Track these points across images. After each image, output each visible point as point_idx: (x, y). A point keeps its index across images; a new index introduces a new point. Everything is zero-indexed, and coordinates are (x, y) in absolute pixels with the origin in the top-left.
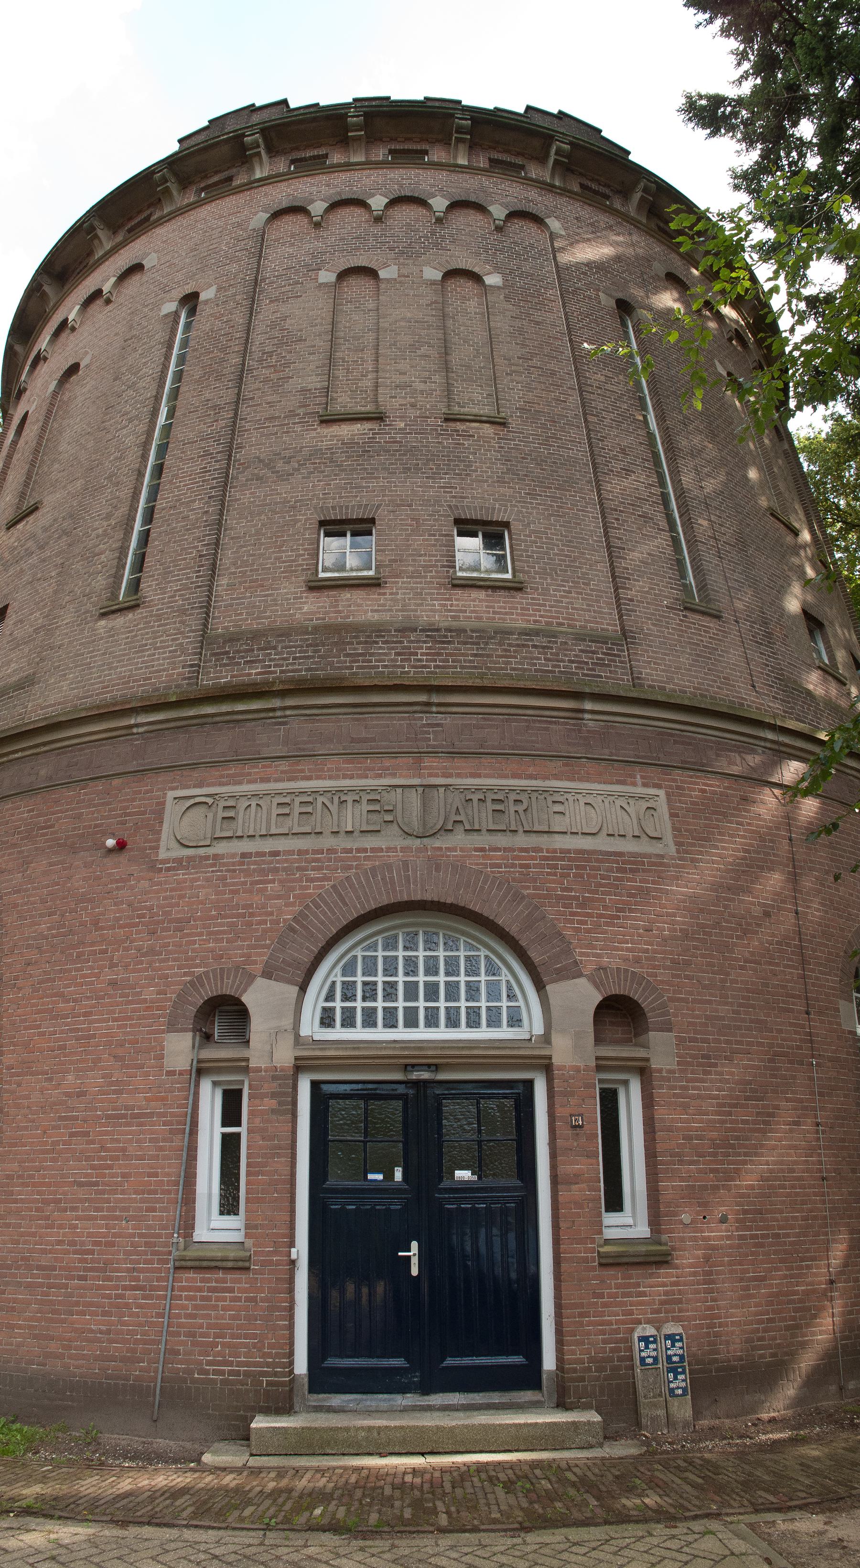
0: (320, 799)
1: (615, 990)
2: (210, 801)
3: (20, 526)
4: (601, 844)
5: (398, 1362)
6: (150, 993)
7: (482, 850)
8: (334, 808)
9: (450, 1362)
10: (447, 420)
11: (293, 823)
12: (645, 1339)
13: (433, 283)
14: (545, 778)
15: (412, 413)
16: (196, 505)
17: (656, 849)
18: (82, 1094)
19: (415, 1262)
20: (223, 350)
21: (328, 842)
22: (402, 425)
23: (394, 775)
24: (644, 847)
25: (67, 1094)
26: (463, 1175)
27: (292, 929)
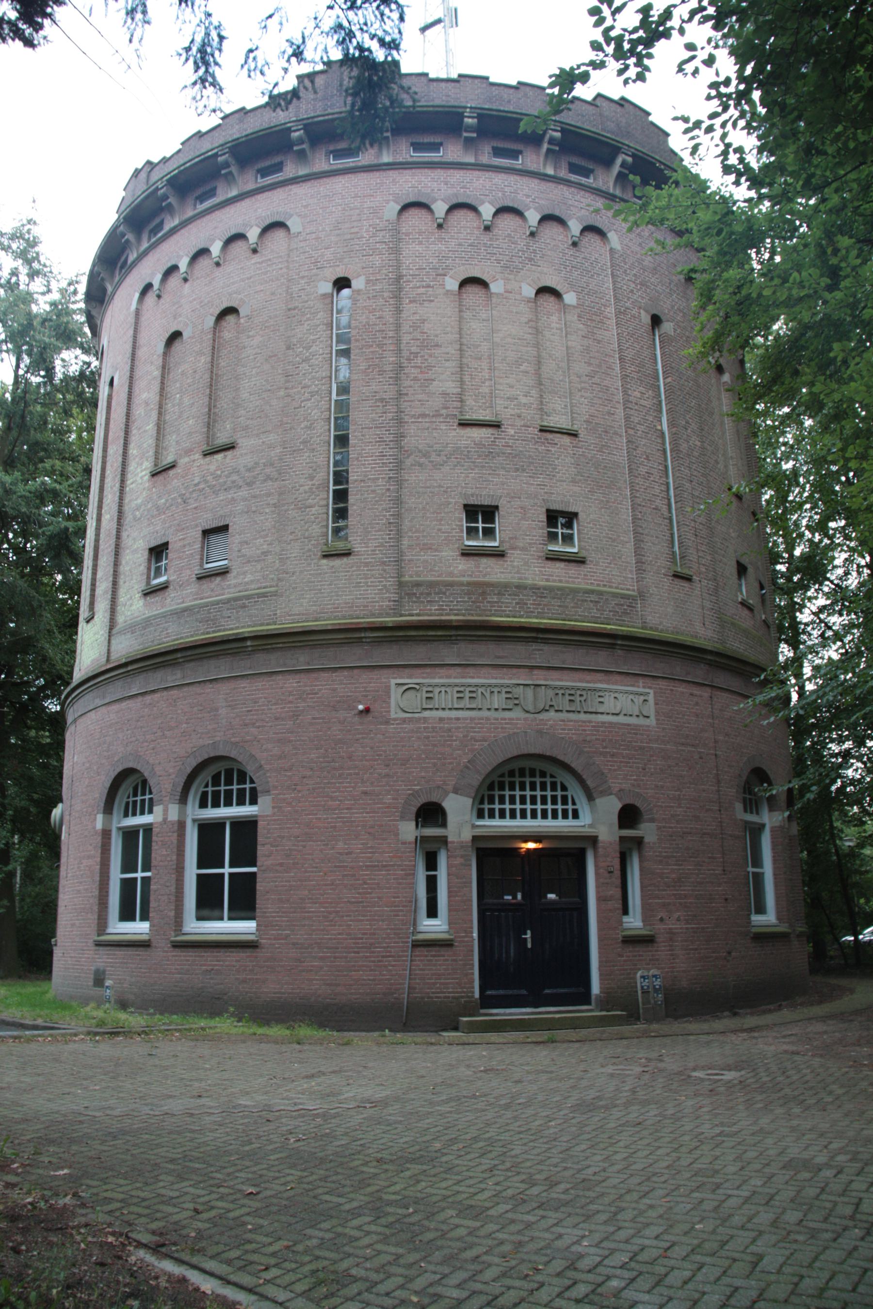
0: (480, 690)
2: (417, 687)
3: (219, 457)
4: (621, 719)
6: (388, 799)
7: (563, 721)
8: (488, 695)
9: (547, 991)
10: (541, 431)
11: (466, 703)
13: (529, 301)
14: (595, 682)
15: (519, 423)
16: (380, 482)
17: (647, 722)
18: (350, 853)
19: (529, 940)
20: (381, 346)
21: (485, 714)
22: (512, 432)
23: (518, 678)
24: (641, 721)
25: (340, 854)
26: (552, 896)
27: (467, 767)
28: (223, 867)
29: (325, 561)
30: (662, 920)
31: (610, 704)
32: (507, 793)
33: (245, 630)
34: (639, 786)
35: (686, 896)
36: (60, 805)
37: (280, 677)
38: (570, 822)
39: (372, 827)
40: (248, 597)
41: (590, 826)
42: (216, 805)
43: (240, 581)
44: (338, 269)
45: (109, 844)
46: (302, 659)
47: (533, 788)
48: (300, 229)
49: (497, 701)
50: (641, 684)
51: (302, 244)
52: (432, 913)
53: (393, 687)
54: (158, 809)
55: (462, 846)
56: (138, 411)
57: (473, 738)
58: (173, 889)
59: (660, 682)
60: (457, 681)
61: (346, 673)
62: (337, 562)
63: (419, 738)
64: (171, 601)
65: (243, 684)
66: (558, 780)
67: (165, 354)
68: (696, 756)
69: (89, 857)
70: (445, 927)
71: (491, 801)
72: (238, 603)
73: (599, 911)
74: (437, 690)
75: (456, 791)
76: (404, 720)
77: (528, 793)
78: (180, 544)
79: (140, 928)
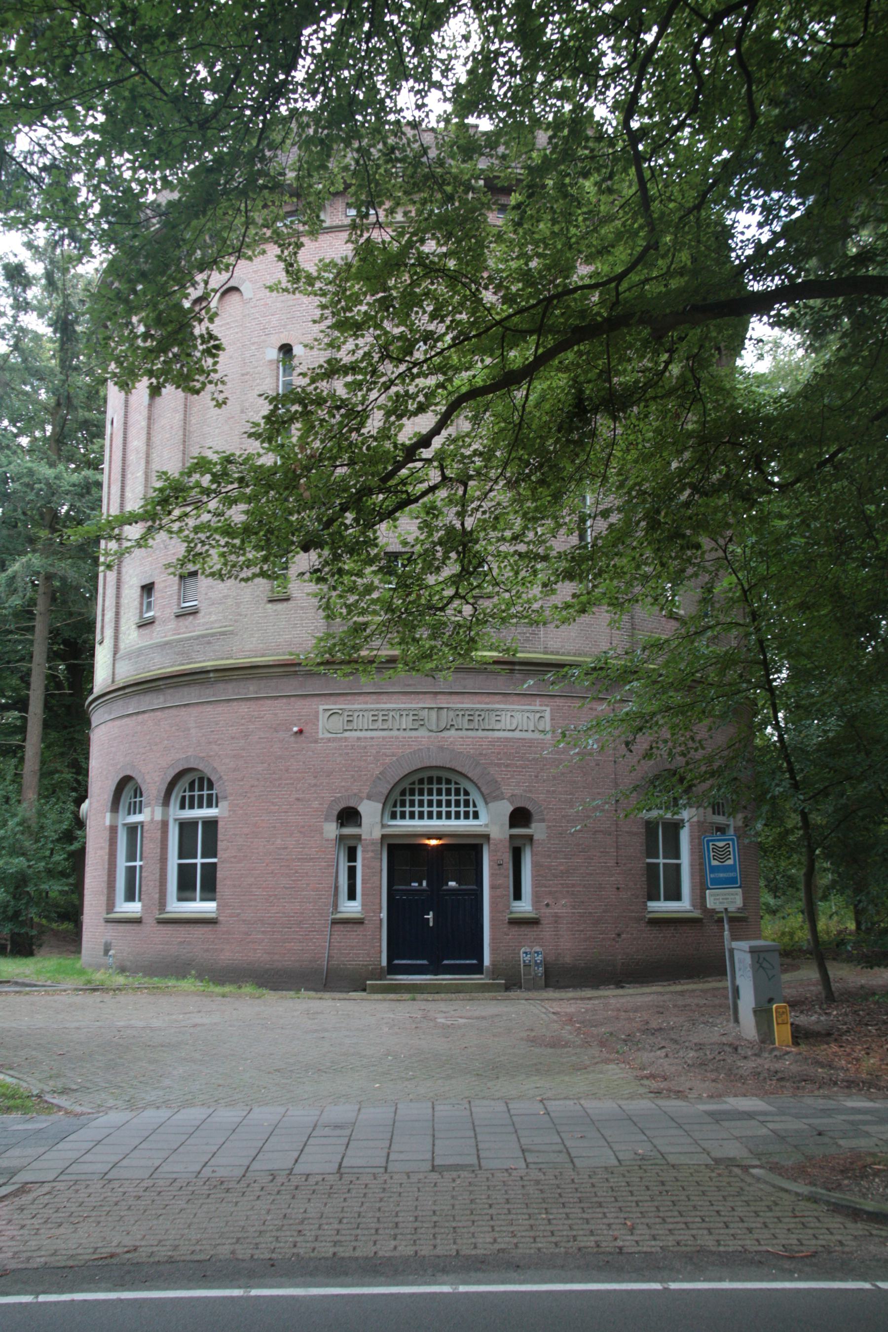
0: (391, 713)
1: (519, 805)
4: (517, 734)
5: (425, 962)
6: (316, 804)
8: (397, 717)
9: (446, 962)
11: (379, 725)
12: (526, 953)
21: (395, 733)
26: (452, 884)
28: (196, 857)
29: (269, 606)
30: (547, 905)
31: (506, 721)
32: (417, 798)
33: (209, 664)
34: (530, 791)
35: (573, 886)
36: (87, 801)
37: (235, 703)
38: (471, 822)
39: (303, 827)
40: (213, 635)
41: (486, 826)
42: (192, 807)
43: (206, 620)
44: (282, 336)
45: (116, 837)
46: (251, 688)
47: (430, 793)
48: (251, 296)
49: (406, 722)
50: (538, 703)
51: (253, 311)
52: (352, 896)
53: (321, 712)
54: (147, 811)
55: (373, 843)
56: (132, 457)
57: (385, 755)
58: (157, 876)
59: (557, 700)
60: (372, 706)
61: (285, 700)
62: (280, 606)
63: (341, 755)
64: (161, 633)
65: (208, 708)
66: (462, 787)
67: (150, 405)
68: (593, 764)
69: (102, 848)
70: (359, 909)
71: (403, 804)
72: (205, 639)
73: (492, 897)
74: (356, 714)
75: (369, 798)
76: (329, 740)
77: (435, 798)
78: (163, 585)
79: (134, 908)
